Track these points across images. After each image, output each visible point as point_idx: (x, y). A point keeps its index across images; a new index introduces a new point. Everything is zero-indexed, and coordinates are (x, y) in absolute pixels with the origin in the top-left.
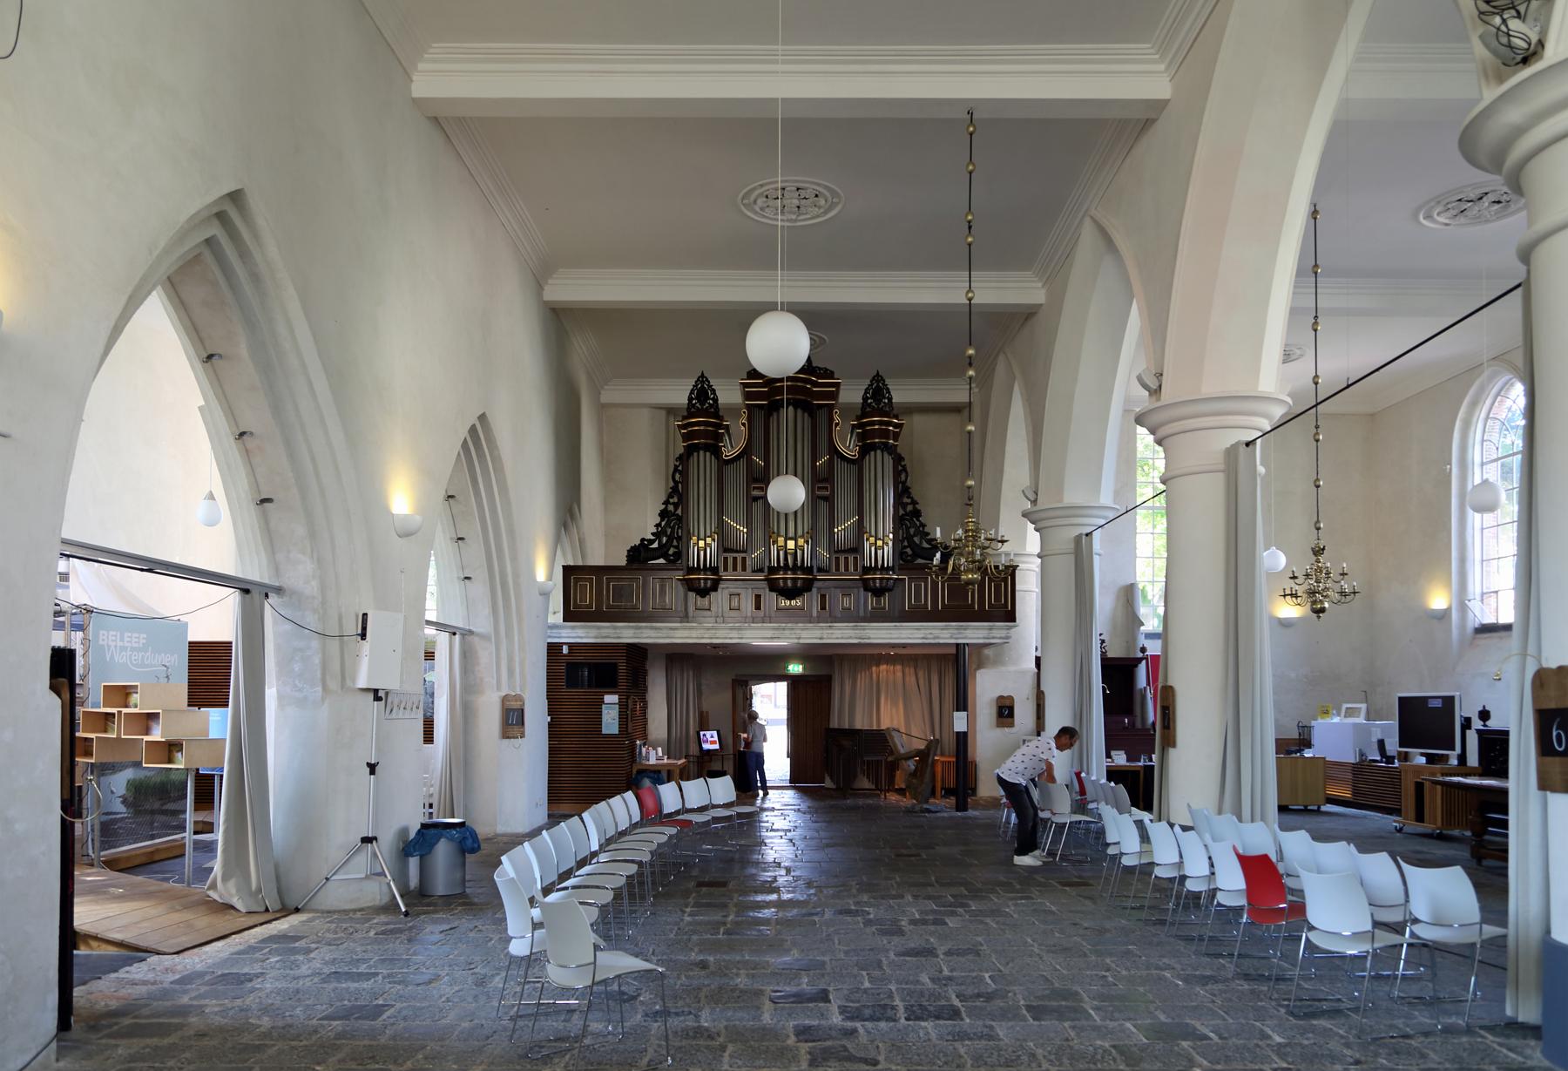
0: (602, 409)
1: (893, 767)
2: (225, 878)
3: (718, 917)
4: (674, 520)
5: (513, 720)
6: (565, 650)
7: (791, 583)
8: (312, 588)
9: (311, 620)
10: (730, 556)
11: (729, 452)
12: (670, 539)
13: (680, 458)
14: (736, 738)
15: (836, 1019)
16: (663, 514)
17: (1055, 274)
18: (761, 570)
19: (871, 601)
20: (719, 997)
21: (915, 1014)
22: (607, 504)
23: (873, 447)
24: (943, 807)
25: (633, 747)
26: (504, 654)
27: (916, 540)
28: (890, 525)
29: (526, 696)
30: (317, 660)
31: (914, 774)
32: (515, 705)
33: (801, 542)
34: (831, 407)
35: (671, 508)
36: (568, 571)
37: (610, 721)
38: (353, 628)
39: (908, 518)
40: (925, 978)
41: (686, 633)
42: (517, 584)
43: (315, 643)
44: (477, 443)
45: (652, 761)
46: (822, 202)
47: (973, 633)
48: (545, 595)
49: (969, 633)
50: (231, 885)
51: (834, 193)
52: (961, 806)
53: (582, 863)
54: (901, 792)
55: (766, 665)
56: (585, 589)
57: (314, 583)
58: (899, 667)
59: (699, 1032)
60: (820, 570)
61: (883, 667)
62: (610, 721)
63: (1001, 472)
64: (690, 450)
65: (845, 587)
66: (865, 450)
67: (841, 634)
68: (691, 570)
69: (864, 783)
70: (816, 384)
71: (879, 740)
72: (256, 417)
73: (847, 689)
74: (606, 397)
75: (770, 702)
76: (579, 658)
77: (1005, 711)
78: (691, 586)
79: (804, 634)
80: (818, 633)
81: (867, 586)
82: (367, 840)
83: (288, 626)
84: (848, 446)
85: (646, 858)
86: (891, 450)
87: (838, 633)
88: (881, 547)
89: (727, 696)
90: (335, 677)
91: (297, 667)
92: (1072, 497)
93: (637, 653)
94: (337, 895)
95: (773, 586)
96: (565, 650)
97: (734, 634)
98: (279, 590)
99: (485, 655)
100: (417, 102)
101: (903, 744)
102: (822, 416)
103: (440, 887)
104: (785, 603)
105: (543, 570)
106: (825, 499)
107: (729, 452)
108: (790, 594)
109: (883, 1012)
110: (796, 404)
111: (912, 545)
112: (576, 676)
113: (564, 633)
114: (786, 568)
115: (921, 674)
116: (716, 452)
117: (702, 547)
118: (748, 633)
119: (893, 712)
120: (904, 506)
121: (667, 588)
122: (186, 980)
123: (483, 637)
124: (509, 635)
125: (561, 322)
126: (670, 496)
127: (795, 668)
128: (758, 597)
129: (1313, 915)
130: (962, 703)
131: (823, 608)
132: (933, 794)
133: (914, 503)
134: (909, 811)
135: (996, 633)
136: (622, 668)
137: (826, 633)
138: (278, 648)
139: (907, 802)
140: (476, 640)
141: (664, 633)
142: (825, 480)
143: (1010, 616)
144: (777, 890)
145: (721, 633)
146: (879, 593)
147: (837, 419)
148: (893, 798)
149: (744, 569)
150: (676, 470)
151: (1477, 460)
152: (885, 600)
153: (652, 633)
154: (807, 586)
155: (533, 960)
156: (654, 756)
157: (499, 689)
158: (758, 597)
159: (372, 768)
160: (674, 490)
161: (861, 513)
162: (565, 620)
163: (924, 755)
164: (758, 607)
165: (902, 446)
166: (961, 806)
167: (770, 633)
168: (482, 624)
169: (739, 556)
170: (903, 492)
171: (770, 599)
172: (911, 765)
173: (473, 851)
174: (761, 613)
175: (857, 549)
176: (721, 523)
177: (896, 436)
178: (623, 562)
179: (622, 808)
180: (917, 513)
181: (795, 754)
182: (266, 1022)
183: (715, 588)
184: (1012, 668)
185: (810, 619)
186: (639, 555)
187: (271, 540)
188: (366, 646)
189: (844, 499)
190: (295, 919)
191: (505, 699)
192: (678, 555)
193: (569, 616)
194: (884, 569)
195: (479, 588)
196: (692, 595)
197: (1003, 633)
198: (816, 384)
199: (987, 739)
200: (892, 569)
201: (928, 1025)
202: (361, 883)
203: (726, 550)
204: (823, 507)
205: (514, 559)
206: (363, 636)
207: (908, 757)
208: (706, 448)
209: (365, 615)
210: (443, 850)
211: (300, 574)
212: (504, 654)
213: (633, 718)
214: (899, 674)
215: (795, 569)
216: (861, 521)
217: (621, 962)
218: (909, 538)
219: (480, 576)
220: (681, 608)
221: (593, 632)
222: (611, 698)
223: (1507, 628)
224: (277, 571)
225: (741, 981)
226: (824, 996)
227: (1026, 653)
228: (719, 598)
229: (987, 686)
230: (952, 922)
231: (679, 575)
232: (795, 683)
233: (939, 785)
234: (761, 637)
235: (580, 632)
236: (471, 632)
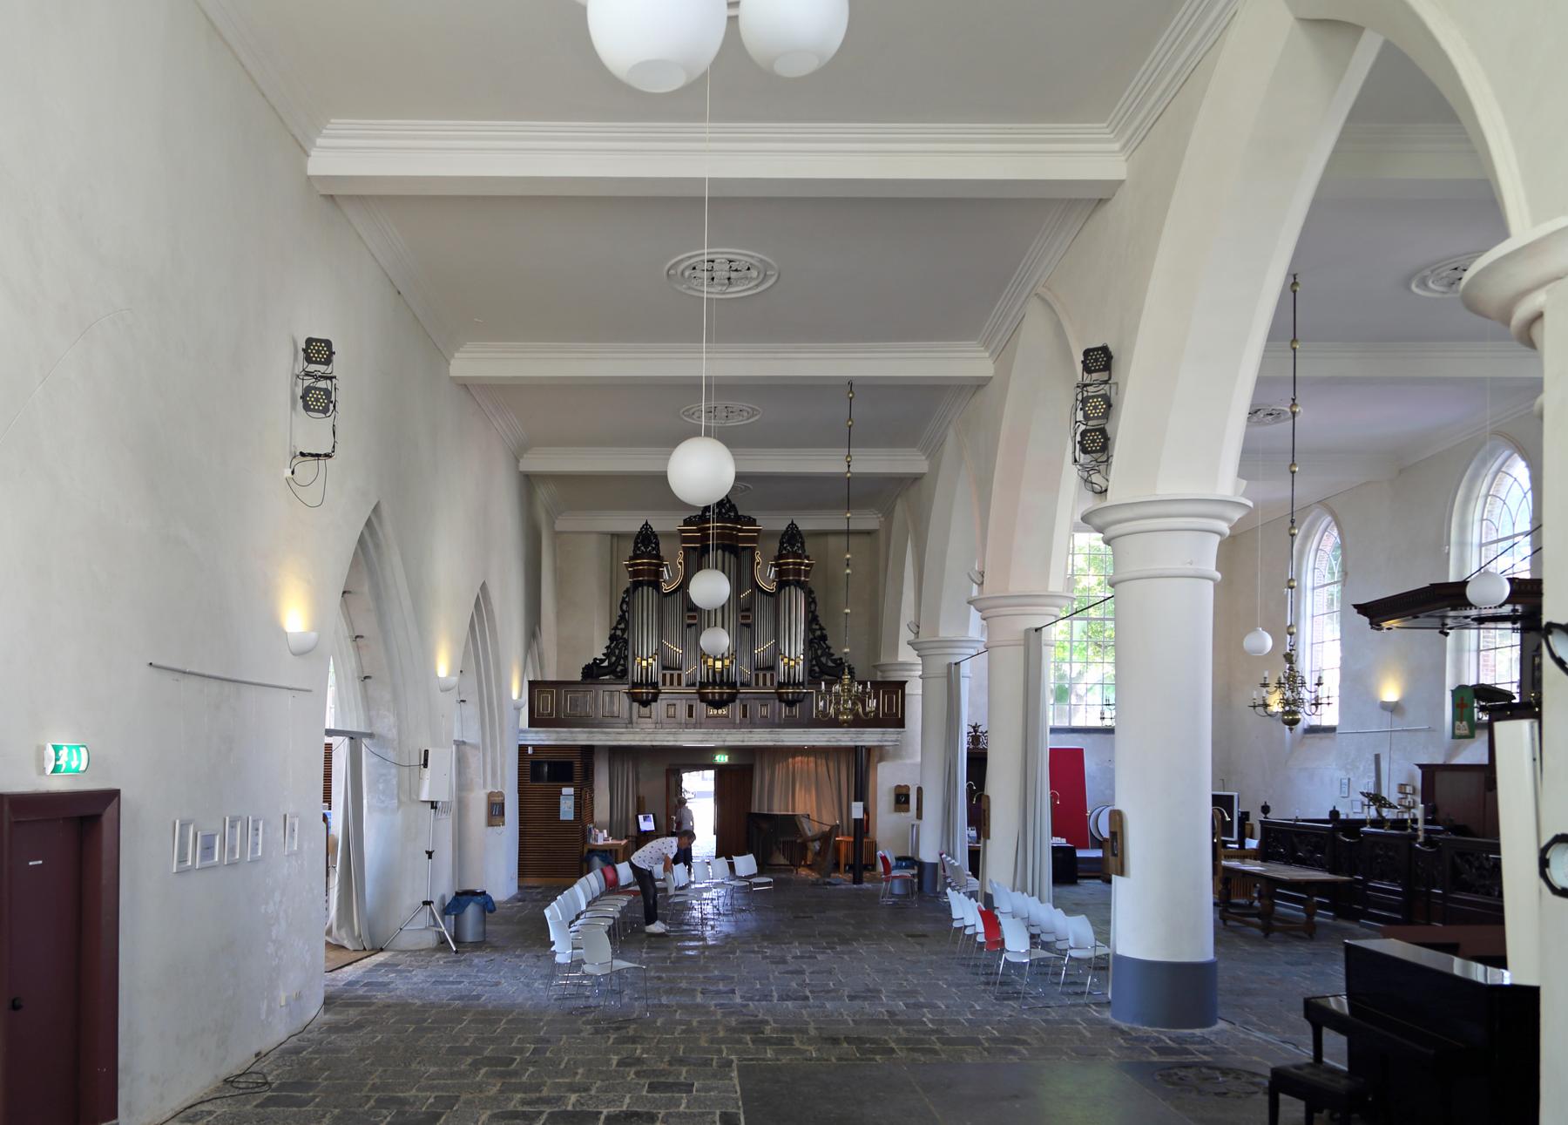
0: (556, 534)
1: (804, 847)
2: (339, 928)
3: (665, 954)
4: (619, 642)
5: (495, 811)
6: (530, 751)
7: (718, 692)
8: (392, 734)
9: (391, 755)
10: (668, 673)
11: (666, 588)
12: (618, 658)
13: (627, 591)
14: (669, 819)
15: (738, 1000)
16: (612, 638)
17: (933, 451)
18: (694, 685)
19: (785, 710)
20: (669, 992)
21: (781, 999)
22: (560, 615)
23: (788, 583)
24: (843, 879)
25: (584, 826)
26: (489, 760)
27: (823, 660)
28: (800, 647)
29: (506, 793)
30: (395, 782)
31: (818, 854)
32: (498, 800)
33: (727, 662)
34: (753, 550)
35: (619, 633)
36: (532, 684)
37: (567, 810)
38: (417, 759)
39: (816, 641)
40: (794, 984)
41: (631, 737)
42: (500, 705)
43: (394, 771)
44: (482, 603)
45: (600, 842)
46: (754, 273)
47: (870, 737)
48: (518, 709)
49: (865, 737)
50: (343, 932)
51: (767, 266)
52: (857, 880)
53: (578, 917)
54: (809, 867)
55: (697, 759)
56: (547, 703)
57: (395, 731)
58: (812, 759)
59: (661, 1005)
60: (742, 684)
61: (798, 759)
62: (567, 810)
63: (901, 593)
64: (636, 585)
65: (763, 699)
66: (782, 584)
67: (760, 738)
68: (635, 685)
69: (781, 860)
70: (740, 530)
71: (790, 823)
72: (366, 626)
73: (767, 778)
74: (559, 526)
75: (699, 788)
76: (542, 757)
77: (900, 798)
78: (634, 698)
79: (729, 738)
80: (740, 737)
81: (781, 698)
82: (426, 903)
83: (376, 759)
84: (766, 577)
85: (617, 916)
86: (799, 584)
87: (757, 737)
88: (794, 653)
89: (660, 783)
90: (406, 794)
91: (381, 787)
92: (945, 633)
93: (588, 752)
94: (407, 940)
95: (703, 698)
96: (530, 751)
97: (671, 738)
98: (371, 736)
99: (474, 761)
100: (453, 378)
101: (810, 829)
102: (745, 556)
103: (470, 935)
104: (713, 712)
105: (517, 691)
106: (748, 626)
107: (666, 588)
108: (718, 704)
109: (766, 997)
110: (724, 548)
111: (819, 664)
112: (544, 772)
113: (529, 736)
114: (714, 684)
115: (831, 765)
116: (656, 586)
117: (645, 662)
118: (683, 737)
119: (808, 803)
120: (813, 631)
121: (615, 698)
122: (350, 984)
123: (475, 747)
124: (493, 745)
125: (529, 482)
126: (619, 623)
127: (722, 759)
128: (691, 707)
129: (1008, 946)
130: (861, 791)
131: (745, 716)
132: (836, 867)
133: (821, 629)
134: (814, 884)
135: (887, 737)
136: (577, 765)
137: (746, 737)
138: (369, 773)
139: (814, 876)
140: (468, 748)
141: (612, 737)
142: (748, 610)
143: (901, 723)
144: (704, 939)
145: (659, 737)
146: (791, 702)
147: (758, 559)
148: (803, 872)
149: (679, 684)
150: (623, 601)
151: (1309, 585)
152: (796, 710)
153: (603, 737)
154: (732, 698)
155: (577, 964)
156: (602, 838)
157: (485, 786)
158: (691, 707)
159: (430, 854)
160: (622, 618)
161: (777, 636)
162: (530, 725)
163: (825, 838)
164: (691, 715)
165: (811, 581)
166: (857, 880)
167: (700, 737)
168: (473, 736)
169: (676, 673)
170: (812, 619)
171: (701, 708)
172: (817, 846)
173: (491, 911)
174: (693, 720)
175: (772, 668)
176: (660, 644)
177: (807, 573)
178: (579, 677)
179: (592, 882)
180: (824, 638)
181: (721, 831)
182: (418, 1002)
183: (655, 699)
184: (908, 761)
185: (733, 725)
186: (592, 672)
187: (368, 702)
188: (427, 773)
189: (763, 627)
190: (380, 958)
191: (490, 795)
192: (625, 672)
193: (534, 722)
194: (797, 685)
195: (472, 709)
196: (636, 705)
197: (894, 737)
198: (740, 530)
199: (887, 825)
200: (802, 684)
201: (790, 1004)
202: (419, 932)
203: (664, 668)
204: (746, 631)
205: (499, 686)
206: (425, 765)
207: (814, 840)
208: (649, 584)
209: (426, 752)
210: (471, 911)
211: (386, 724)
212: (489, 760)
213: (583, 804)
214: (812, 765)
215: (721, 684)
216: (777, 644)
217: (621, 964)
218: (817, 658)
219: (473, 699)
220: (626, 715)
221: (554, 736)
222: (568, 791)
223: (1332, 729)
224: (370, 721)
225: (684, 985)
226: (733, 992)
227: (912, 759)
228: (659, 707)
229: (886, 778)
230: (819, 957)
231: (625, 688)
232: (721, 771)
233: (843, 862)
234: (689, 739)
235: (543, 736)
236: (464, 743)
